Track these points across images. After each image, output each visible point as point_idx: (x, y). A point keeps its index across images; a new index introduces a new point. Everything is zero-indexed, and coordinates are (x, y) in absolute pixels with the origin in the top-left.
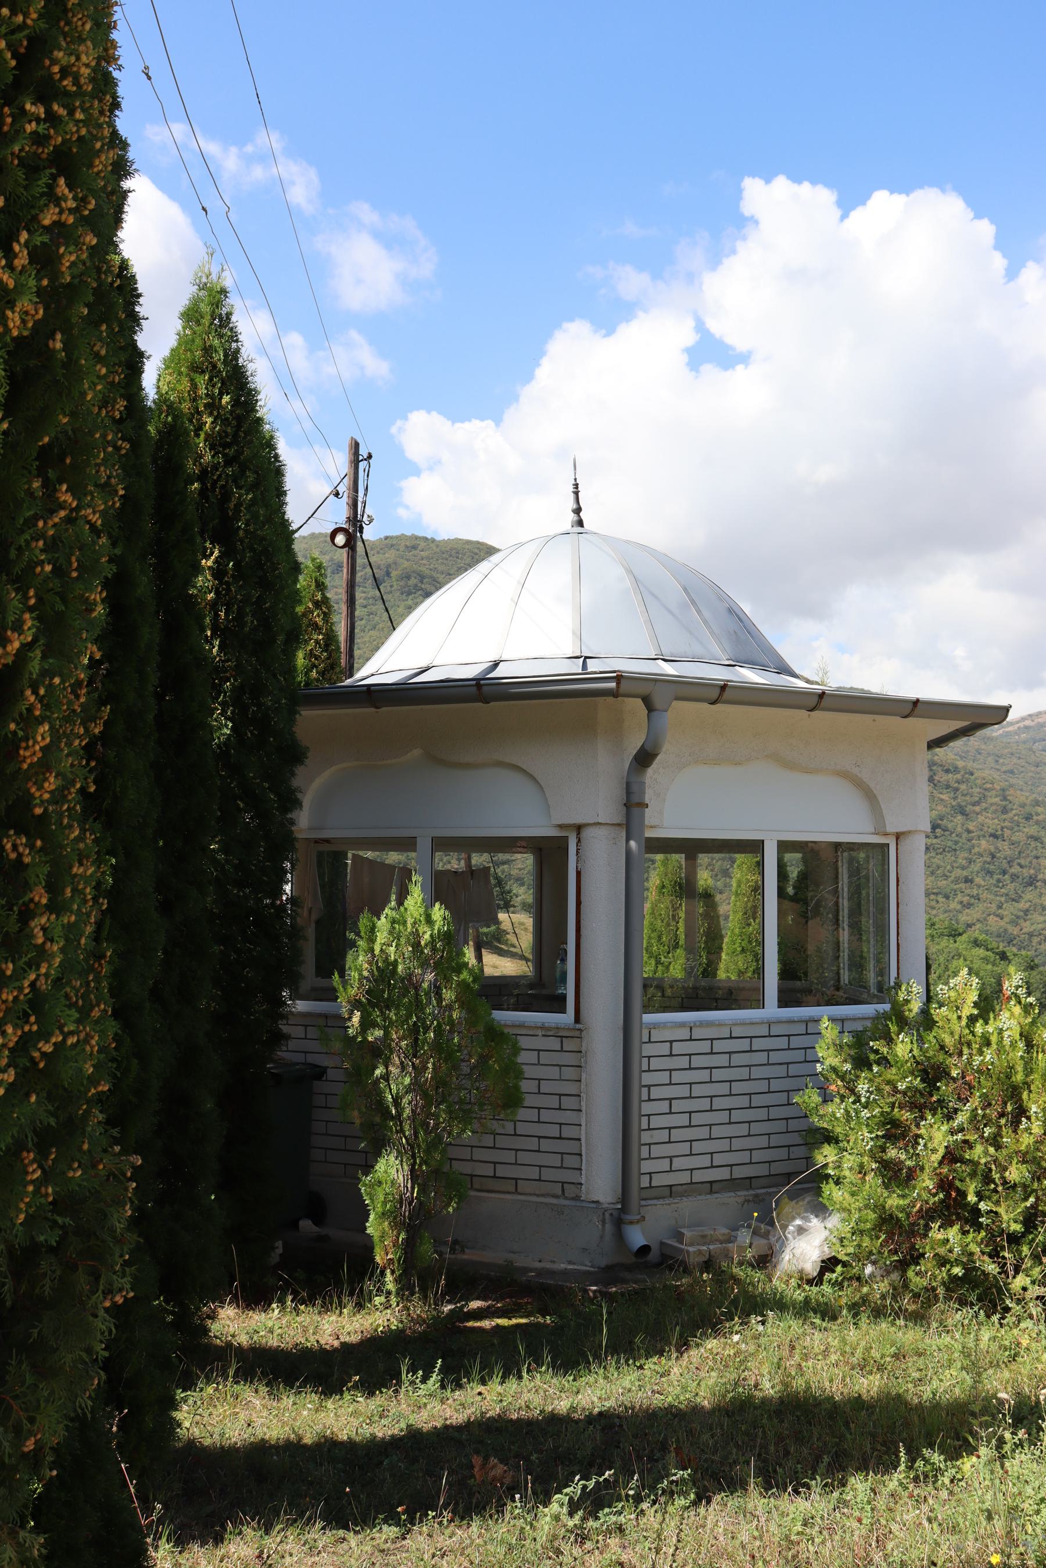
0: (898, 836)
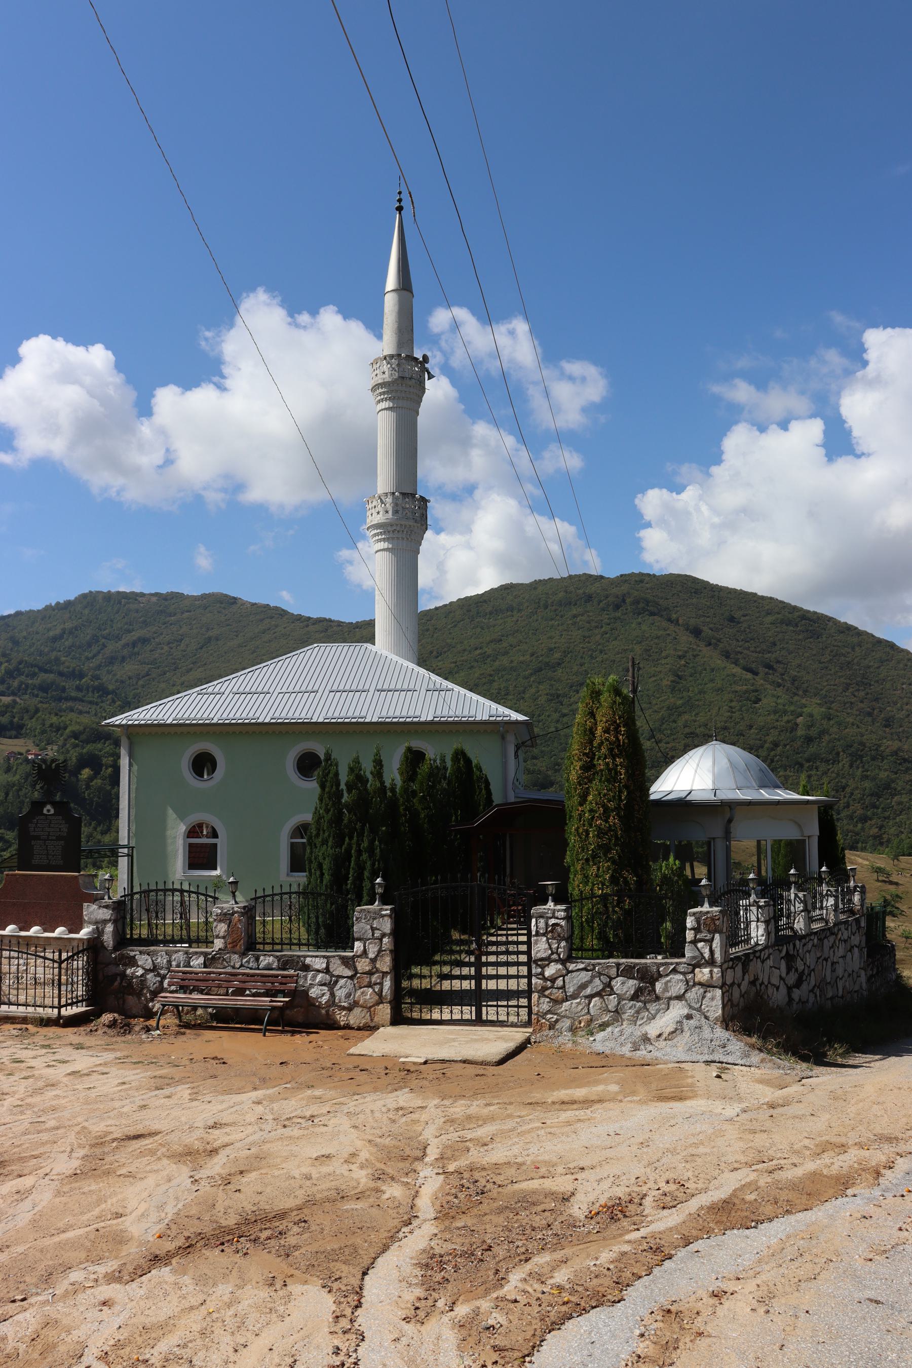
0: (809, 837)
